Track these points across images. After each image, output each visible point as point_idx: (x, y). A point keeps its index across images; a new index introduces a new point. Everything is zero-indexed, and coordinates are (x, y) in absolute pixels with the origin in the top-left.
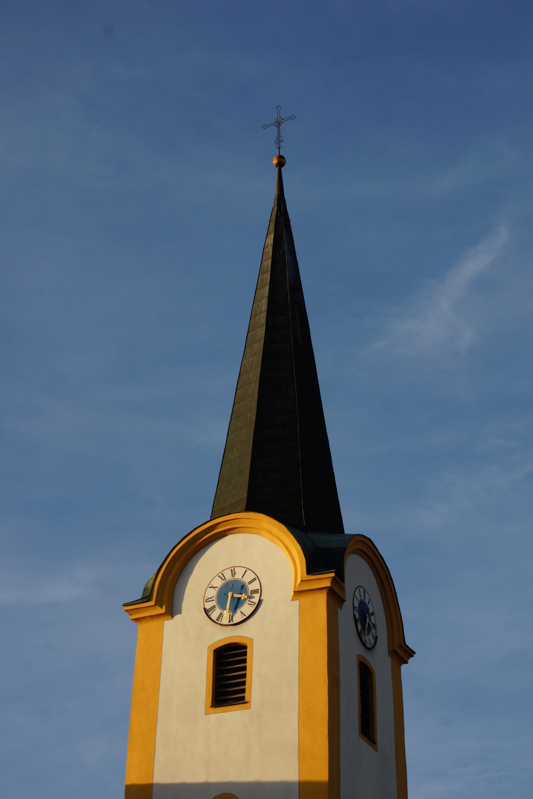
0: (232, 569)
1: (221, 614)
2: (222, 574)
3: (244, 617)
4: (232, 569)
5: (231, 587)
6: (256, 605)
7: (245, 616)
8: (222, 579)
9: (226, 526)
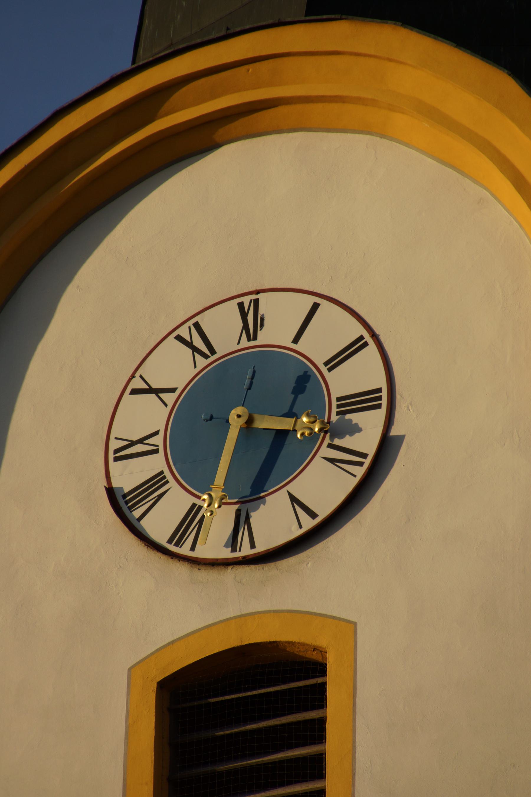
0: (246, 300)
1: (194, 509)
2: (197, 325)
3: (308, 523)
4: (246, 300)
5: (247, 382)
6: (367, 462)
7: (313, 515)
8: (195, 350)
9: (214, 96)
